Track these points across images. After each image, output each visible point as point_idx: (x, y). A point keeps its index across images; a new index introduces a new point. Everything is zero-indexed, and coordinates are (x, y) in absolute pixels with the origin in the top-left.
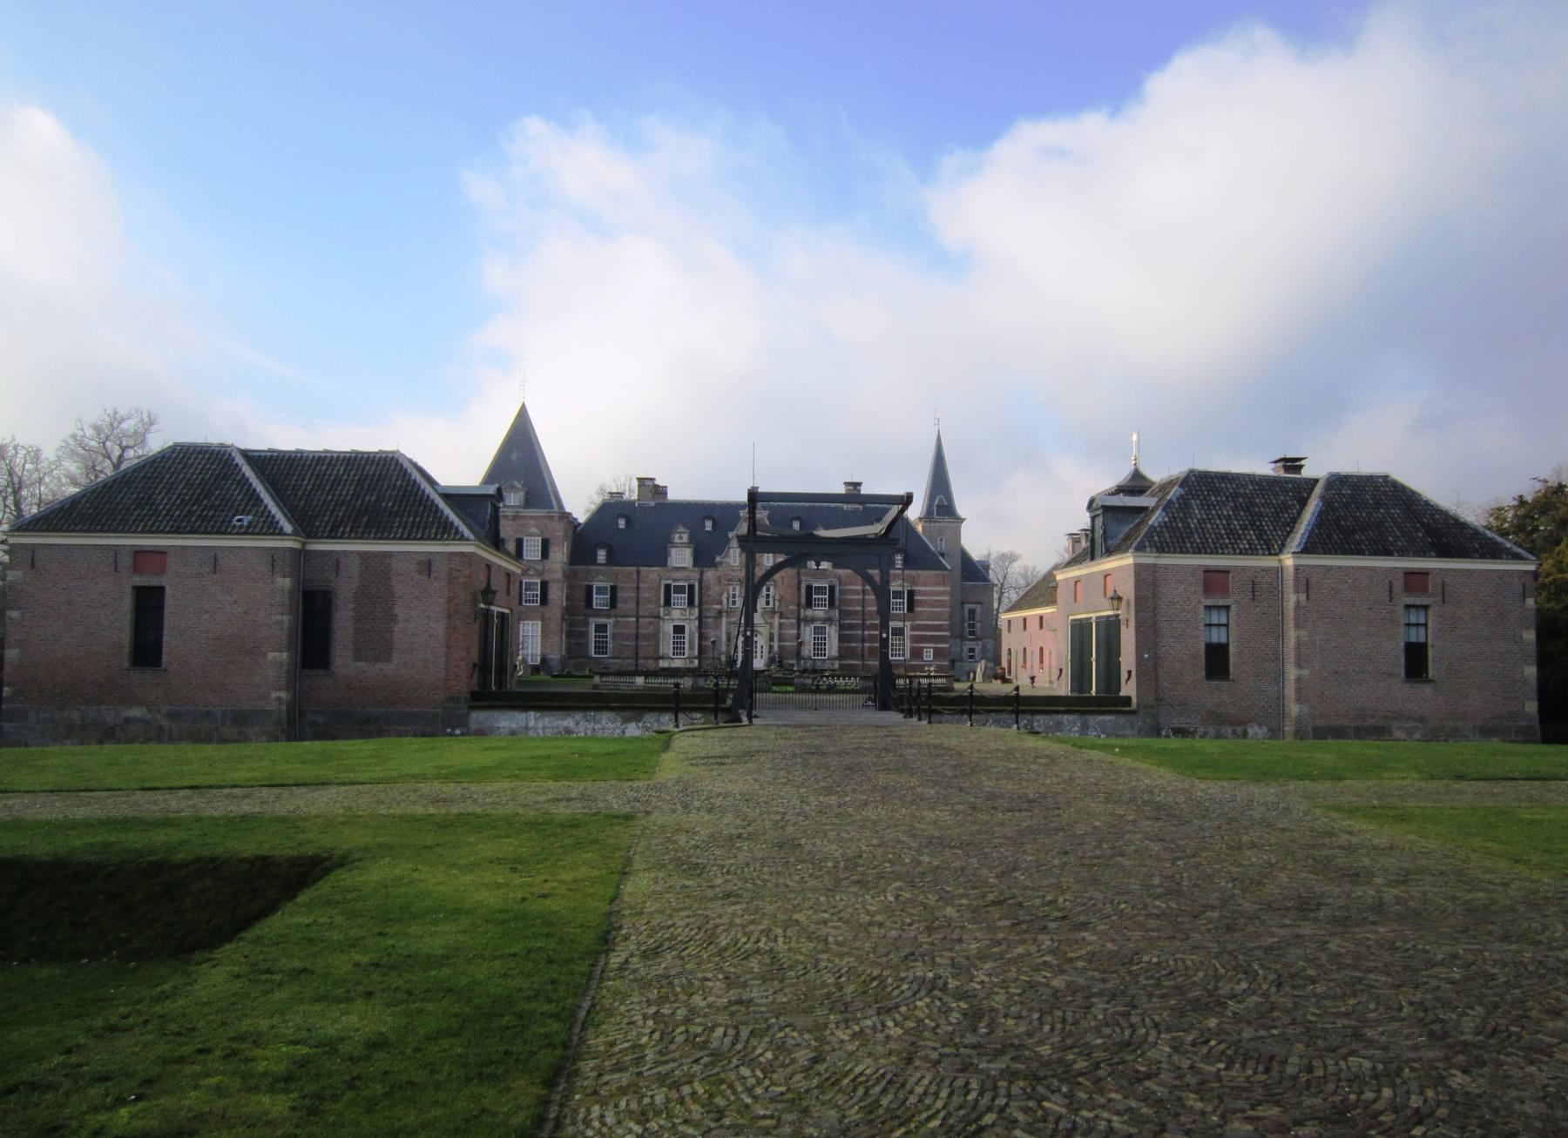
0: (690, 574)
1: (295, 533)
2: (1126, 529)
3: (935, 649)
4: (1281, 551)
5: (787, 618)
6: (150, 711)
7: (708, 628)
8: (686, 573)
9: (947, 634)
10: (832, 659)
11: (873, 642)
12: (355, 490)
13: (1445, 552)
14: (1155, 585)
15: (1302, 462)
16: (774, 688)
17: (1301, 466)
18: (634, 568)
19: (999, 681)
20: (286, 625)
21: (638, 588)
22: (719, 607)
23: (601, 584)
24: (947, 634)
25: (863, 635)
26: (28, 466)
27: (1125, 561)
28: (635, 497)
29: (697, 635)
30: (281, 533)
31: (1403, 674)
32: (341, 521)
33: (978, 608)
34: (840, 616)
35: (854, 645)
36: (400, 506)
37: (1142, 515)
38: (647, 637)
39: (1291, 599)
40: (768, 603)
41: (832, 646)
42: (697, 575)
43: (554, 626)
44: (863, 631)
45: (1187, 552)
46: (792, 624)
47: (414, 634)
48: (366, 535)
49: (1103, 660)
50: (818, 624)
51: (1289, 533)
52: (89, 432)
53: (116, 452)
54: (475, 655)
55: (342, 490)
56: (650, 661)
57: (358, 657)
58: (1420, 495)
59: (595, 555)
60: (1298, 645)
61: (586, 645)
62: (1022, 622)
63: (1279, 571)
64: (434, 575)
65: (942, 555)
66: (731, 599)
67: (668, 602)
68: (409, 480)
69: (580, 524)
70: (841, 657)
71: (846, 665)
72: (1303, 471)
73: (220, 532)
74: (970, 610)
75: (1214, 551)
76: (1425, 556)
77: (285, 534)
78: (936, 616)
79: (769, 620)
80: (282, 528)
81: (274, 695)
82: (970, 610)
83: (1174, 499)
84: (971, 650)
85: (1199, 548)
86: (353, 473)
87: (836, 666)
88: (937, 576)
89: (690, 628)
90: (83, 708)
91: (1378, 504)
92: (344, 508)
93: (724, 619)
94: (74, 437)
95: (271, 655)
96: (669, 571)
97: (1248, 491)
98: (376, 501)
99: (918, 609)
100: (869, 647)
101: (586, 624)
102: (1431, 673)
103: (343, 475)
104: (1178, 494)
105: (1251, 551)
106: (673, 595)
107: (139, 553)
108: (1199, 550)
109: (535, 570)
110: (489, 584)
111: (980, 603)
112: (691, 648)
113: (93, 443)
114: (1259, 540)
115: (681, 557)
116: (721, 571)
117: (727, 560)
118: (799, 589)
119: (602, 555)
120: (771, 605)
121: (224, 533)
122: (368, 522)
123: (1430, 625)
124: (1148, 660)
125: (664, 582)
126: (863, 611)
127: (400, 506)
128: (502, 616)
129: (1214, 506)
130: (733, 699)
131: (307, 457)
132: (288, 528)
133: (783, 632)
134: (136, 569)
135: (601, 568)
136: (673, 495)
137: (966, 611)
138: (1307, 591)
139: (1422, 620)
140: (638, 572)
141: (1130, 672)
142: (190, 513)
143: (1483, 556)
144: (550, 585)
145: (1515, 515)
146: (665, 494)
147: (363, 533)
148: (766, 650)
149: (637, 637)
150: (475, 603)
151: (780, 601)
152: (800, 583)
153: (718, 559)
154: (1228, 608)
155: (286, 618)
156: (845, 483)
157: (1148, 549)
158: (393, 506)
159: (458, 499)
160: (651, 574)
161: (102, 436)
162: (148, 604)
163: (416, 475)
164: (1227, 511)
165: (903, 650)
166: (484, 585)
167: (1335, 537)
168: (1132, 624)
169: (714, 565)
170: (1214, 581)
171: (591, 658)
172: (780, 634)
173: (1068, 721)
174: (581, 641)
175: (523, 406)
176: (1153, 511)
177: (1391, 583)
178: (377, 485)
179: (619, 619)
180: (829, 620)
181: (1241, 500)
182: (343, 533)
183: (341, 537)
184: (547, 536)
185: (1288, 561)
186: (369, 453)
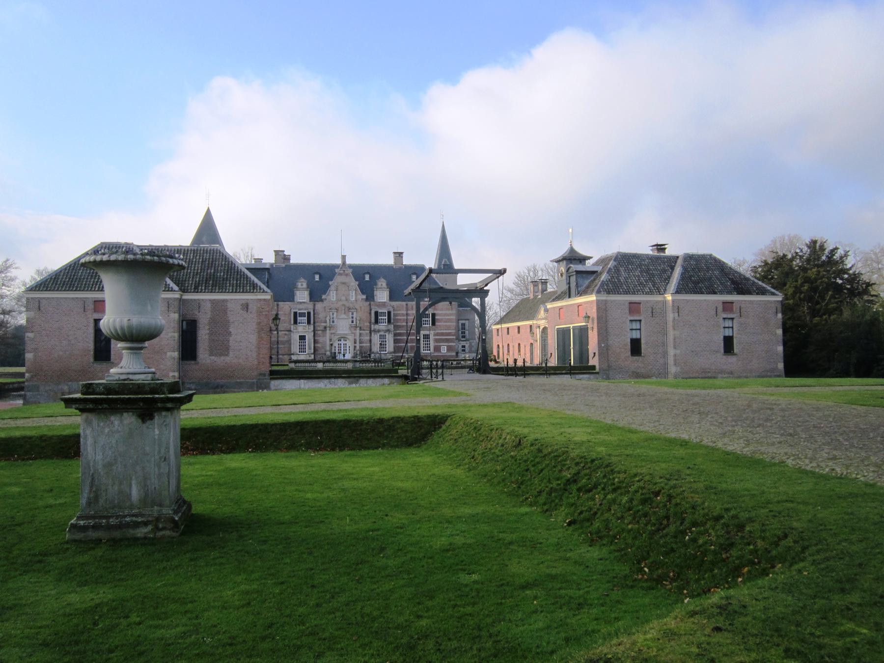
2: (587, 282)
3: (448, 346)
5: (364, 330)
7: (320, 336)
9: (454, 337)
11: (413, 343)
12: (201, 267)
13: (741, 292)
15: (666, 246)
17: (665, 249)
18: (404, 303)
22: (325, 324)
24: (454, 337)
27: (593, 298)
28: (273, 261)
29: (313, 340)
31: (722, 350)
32: (199, 283)
33: (467, 323)
36: (227, 275)
37: (595, 275)
38: (283, 343)
39: (670, 316)
40: (353, 322)
41: (390, 346)
45: (621, 294)
47: (241, 341)
48: (213, 291)
49: (577, 347)
50: (382, 333)
51: (667, 283)
55: (195, 267)
56: (285, 356)
62: (506, 330)
63: (665, 302)
64: (249, 311)
66: (331, 320)
67: (295, 322)
68: (229, 262)
72: (666, 251)
74: (462, 324)
75: (634, 293)
76: (732, 294)
77: (175, 291)
78: (448, 328)
80: (172, 288)
82: (462, 324)
83: (612, 267)
84: (464, 347)
86: (198, 257)
90: (70, 383)
91: (708, 269)
92: (198, 276)
93: (328, 331)
95: (169, 354)
97: (646, 263)
98: (214, 272)
102: (736, 351)
103: (193, 259)
104: (613, 265)
105: (651, 293)
106: (298, 318)
108: (627, 293)
111: (468, 320)
112: (310, 348)
114: (654, 287)
115: (302, 296)
116: (325, 304)
117: (329, 297)
122: (213, 284)
123: (734, 327)
125: (293, 311)
127: (227, 275)
131: (171, 249)
132: (176, 288)
137: (460, 324)
140: (278, 305)
145: (762, 271)
146: (289, 259)
147: (212, 289)
148: (352, 348)
151: (360, 320)
152: (371, 310)
153: (324, 297)
154: (640, 321)
156: (394, 253)
157: (603, 293)
158: (224, 275)
164: (637, 273)
165: (430, 347)
168: (596, 330)
169: (322, 301)
172: (360, 340)
175: (208, 213)
176: (601, 273)
178: (212, 264)
180: (388, 331)
181: (643, 267)
182: (202, 289)
185: (669, 297)
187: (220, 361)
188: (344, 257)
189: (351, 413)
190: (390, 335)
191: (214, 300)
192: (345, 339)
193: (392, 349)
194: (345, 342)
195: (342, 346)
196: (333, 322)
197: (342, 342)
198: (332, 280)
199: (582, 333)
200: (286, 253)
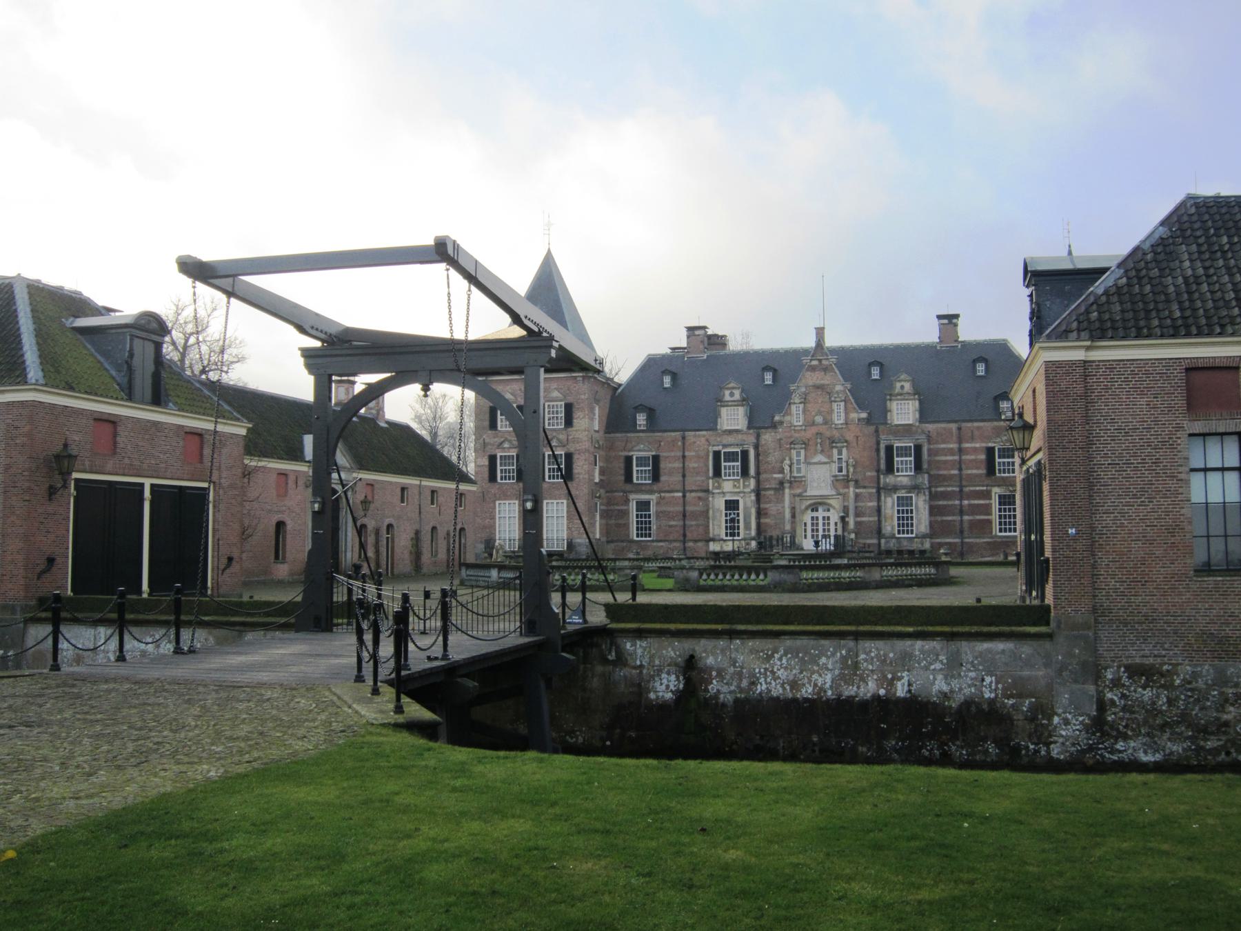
0: (745, 437)
5: (865, 487)
7: (770, 502)
8: (740, 436)
10: (924, 536)
21: (684, 457)
25: (961, 505)
29: (753, 511)
34: (930, 482)
35: (950, 518)
38: (695, 515)
40: (840, 470)
42: (752, 439)
44: (961, 500)
46: (870, 494)
50: (903, 494)
61: (626, 526)
66: (795, 466)
67: (717, 473)
70: (931, 535)
79: (842, 491)
85: (1176, 328)
89: (745, 504)
93: (787, 491)
96: (720, 435)
101: (627, 501)
112: (747, 527)
115: (733, 418)
117: (787, 418)
118: (878, 450)
119: (641, 419)
120: (844, 472)
124: (1074, 539)
126: (960, 475)
129: (1224, 252)
133: (860, 504)
135: (641, 434)
136: (735, 345)
140: (684, 438)
144: (576, 457)
149: (684, 516)
152: (878, 443)
156: (939, 317)
169: (774, 426)
171: (633, 541)
173: (922, 651)
174: (621, 522)
175: (549, 253)
179: (663, 494)
180: (915, 488)
184: (570, 399)
188: (820, 332)
197: (821, 514)
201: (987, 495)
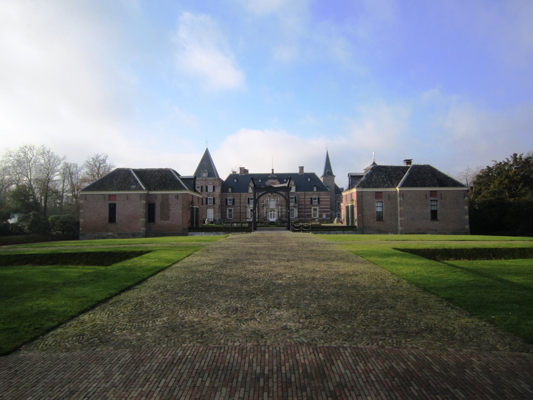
1: (146, 190)
3: (326, 214)
4: (396, 186)
6: (113, 233)
10: (296, 218)
14: (362, 196)
16: (270, 226)
17: (411, 162)
18: (239, 193)
19: (340, 223)
20: (144, 212)
21: (240, 199)
23: (230, 198)
26: (74, 169)
28: (239, 173)
30: (143, 190)
40: (277, 202)
43: (217, 210)
45: (371, 188)
52: (91, 160)
53: (98, 165)
54: (189, 218)
57: (161, 219)
58: (437, 170)
59: (228, 190)
60: (401, 211)
61: (226, 215)
63: (397, 191)
65: (328, 187)
67: (249, 203)
69: (224, 181)
71: (300, 220)
73: (128, 190)
75: (378, 187)
78: (326, 205)
81: (142, 229)
87: (297, 220)
88: (326, 193)
94: (87, 161)
99: (321, 203)
100: (307, 214)
101: (226, 209)
102: (438, 218)
105: (389, 187)
107: (110, 195)
108: (374, 187)
109: (212, 195)
110: (193, 201)
113: (92, 163)
119: (230, 190)
120: (278, 203)
121: (129, 190)
123: (438, 205)
128: (197, 209)
130: (42, 204)
132: (144, 188)
134: (109, 199)
136: (250, 172)
138: (403, 197)
139: (436, 204)
140: (240, 194)
141: (356, 219)
142: (121, 186)
143: (452, 186)
150: (189, 205)
151: (281, 202)
155: (144, 210)
159: (186, 180)
160: (244, 195)
161: (94, 161)
162: (112, 209)
163: (174, 174)
166: (191, 201)
167: (411, 182)
168: (356, 207)
170: (378, 195)
171: (228, 219)
172: (281, 211)
177: (426, 194)
180: (295, 207)
182: (157, 189)
183: (157, 190)
184: (214, 185)
185: (398, 189)
186: (163, 169)
187: (166, 222)
188: (273, 170)
189: (122, 249)
190: (296, 209)
191: (163, 194)
192: (274, 211)
193: (297, 216)
194: (274, 213)
195: (272, 214)
196: (268, 202)
197: (272, 212)
198: (267, 182)
199: (352, 207)
200: (245, 168)
201: (311, 208)
